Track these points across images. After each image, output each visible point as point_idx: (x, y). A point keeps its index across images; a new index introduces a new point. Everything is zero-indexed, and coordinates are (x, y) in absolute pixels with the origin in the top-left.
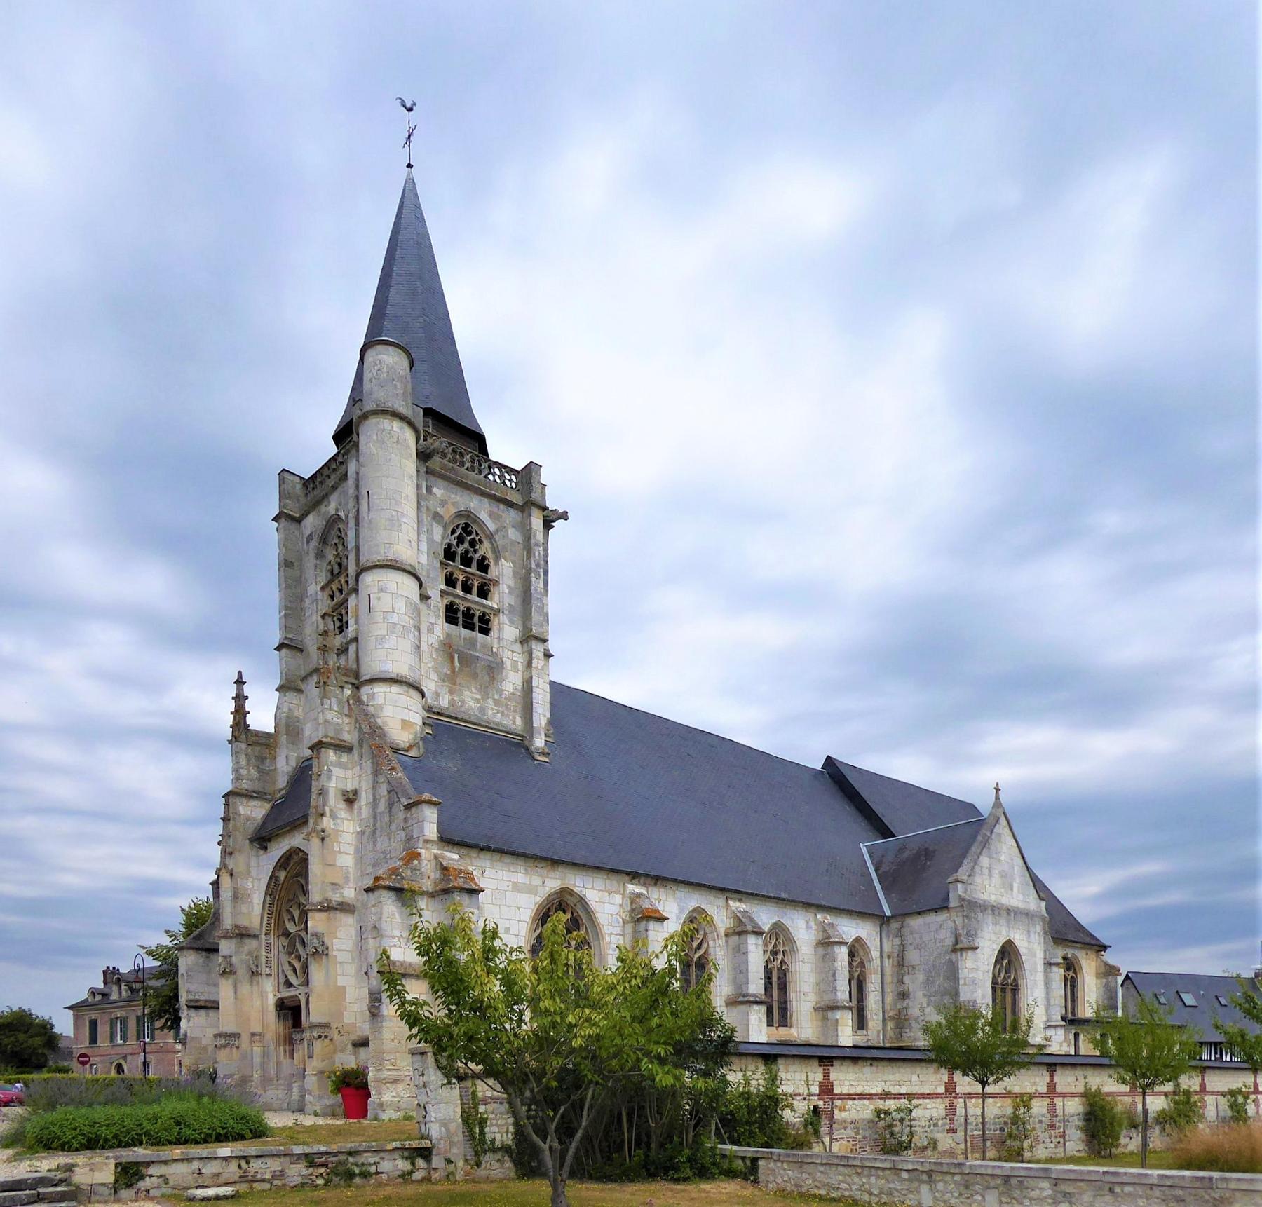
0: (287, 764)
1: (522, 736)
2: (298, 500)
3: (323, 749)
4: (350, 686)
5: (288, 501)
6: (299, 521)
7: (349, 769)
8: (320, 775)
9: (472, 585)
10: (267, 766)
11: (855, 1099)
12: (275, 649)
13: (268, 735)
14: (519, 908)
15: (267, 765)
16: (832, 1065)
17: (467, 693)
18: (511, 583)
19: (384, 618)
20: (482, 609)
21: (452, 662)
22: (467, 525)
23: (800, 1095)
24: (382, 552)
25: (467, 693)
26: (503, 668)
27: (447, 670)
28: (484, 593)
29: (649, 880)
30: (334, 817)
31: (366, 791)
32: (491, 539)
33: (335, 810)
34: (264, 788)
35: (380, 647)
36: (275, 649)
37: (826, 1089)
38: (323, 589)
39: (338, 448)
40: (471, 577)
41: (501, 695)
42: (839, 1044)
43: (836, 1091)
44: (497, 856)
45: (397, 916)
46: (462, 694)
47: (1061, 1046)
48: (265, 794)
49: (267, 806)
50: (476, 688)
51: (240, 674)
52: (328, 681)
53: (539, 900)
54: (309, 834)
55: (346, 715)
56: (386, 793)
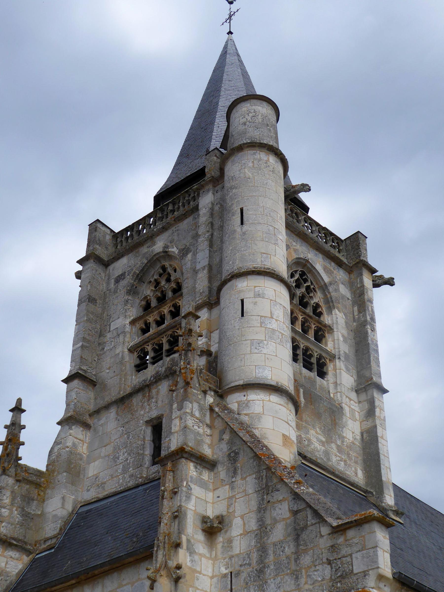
0: (63, 507)
1: (366, 492)
2: (107, 248)
3: (183, 460)
4: (212, 393)
5: (97, 246)
6: (106, 264)
7: (209, 490)
8: (175, 493)
9: (310, 328)
10: (33, 509)
12: (62, 381)
13: (39, 473)
15: (33, 508)
17: (312, 432)
18: (345, 332)
19: (261, 323)
20: (319, 352)
24: (259, 260)
25: (312, 432)
30: (191, 551)
31: (242, 517)
32: (324, 291)
33: (192, 541)
34: (25, 537)
35: (256, 351)
36: (62, 381)
38: (133, 323)
39: (82, 266)
40: (309, 319)
48: (26, 543)
49: (26, 559)
50: (321, 428)
51: (19, 401)
52: (191, 382)
54: (157, 571)
55: (207, 425)
56: (287, 515)
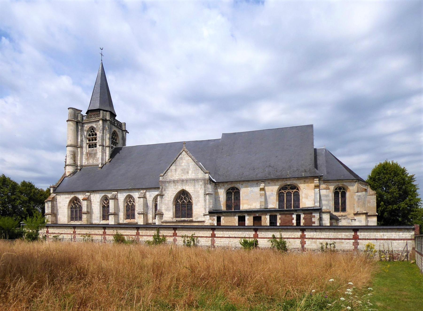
21: (88, 156)
22: (93, 128)
28: (96, 140)
29: (92, 192)
37: (47, 232)
44: (63, 193)
53: (70, 199)
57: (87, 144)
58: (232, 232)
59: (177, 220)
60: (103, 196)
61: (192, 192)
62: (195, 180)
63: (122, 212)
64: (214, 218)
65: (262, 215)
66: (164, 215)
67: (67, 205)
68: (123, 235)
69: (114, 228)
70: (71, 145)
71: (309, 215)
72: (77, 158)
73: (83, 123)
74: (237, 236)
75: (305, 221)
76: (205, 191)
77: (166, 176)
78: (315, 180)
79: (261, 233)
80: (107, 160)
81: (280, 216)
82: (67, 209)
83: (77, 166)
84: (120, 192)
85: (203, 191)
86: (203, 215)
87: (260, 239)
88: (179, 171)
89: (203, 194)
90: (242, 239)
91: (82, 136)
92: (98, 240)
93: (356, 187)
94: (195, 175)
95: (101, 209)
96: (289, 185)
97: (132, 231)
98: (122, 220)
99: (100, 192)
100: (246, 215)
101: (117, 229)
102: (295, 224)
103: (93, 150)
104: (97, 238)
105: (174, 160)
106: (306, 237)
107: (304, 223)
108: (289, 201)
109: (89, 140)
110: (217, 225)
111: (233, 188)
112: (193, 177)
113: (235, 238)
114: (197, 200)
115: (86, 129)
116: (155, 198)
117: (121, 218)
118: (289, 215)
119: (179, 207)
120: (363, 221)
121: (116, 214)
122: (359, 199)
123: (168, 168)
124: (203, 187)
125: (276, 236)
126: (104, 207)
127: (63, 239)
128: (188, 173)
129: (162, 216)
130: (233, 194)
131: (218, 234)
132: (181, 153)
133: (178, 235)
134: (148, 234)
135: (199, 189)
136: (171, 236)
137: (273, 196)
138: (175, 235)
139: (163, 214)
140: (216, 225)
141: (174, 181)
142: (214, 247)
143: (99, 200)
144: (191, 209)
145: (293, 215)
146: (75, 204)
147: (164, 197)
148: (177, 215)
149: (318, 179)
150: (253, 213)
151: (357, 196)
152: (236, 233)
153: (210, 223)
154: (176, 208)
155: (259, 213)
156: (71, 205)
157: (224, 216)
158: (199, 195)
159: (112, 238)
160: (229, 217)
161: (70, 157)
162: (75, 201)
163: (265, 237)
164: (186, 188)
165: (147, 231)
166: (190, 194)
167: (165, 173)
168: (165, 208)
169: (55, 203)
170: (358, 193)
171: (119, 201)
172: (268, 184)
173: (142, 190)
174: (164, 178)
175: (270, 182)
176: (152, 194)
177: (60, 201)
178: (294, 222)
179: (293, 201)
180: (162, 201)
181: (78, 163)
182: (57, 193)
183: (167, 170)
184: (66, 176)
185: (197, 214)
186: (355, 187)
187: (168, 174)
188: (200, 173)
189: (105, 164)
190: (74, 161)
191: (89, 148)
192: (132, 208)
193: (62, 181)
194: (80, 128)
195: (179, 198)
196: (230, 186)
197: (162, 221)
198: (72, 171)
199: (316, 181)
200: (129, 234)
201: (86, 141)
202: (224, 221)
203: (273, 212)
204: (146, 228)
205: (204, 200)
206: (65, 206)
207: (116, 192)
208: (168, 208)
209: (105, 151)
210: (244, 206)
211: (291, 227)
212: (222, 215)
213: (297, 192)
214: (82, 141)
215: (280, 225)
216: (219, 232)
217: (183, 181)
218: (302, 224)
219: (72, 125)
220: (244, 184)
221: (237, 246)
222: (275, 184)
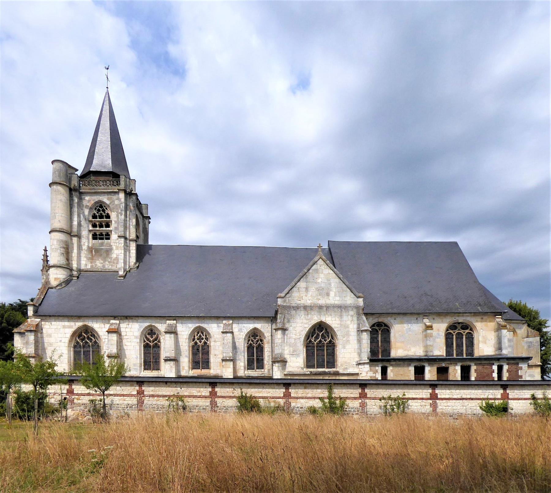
11: (85, 395)
14: (65, 333)
16: (73, 383)
22: (101, 205)
23: (57, 393)
26: (112, 249)
27: (90, 256)
28: (108, 226)
29: (122, 318)
41: (111, 259)
42: (165, 376)
43: (75, 392)
45: (19, 340)
46: (95, 262)
47: (367, 374)
50: (101, 259)
53: (73, 330)
57: (90, 231)
58: (465, 391)
59: (311, 372)
60: (146, 327)
61: (336, 326)
62: (341, 308)
63: (186, 356)
64: (377, 368)
65: (450, 365)
66: (288, 363)
67: (67, 340)
68: (255, 397)
69: (227, 384)
70: (61, 229)
71: (514, 367)
72: (70, 255)
73: (81, 193)
74: (474, 397)
75: (509, 375)
76: (359, 326)
77: (290, 298)
78: (497, 318)
79: (513, 391)
80: (133, 263)
81: (475, 366)
82: (66, 348)
83: (71, 270)
84: (180, 321)
85: (355, 326)
86: (355, 364)
87: (511, 401)
88: (312, 291)
89: (356, 330)
90: (484, 402)
91: (79, 216)
92: (196, 406)
93: (524, 330)
94: (341, 299)
95: (141, 350)
96: (459, 323)
97: (274, 390)
98: (186, 370)
99: (141, 320)
100: (426, 365)
101: (242, 387)
102: (496, 379)
103: (102, 244)
104: (196, 404)
105: (303, 273)
106: (439, 397)
107: (507, 378)
108: (460, 346)
109: (94, 226)
110: (382, 379)
111: (379, 324)
112: (336, 302)
113: (472, 399)
114: (344, 339)
115: (88, 204)
116: (248, 335)
117: (183, 367)
118: (488, 365)
119: (312, 351)
120: (536, 376)
121: (175, 360)
122: (529, 347)
123: (294, 284)
124: (355, 319)
125: (536, 396)
126: (146, 346)
127: (111, 407)
128: (328, 294)
129: (285, 365)
130: (380, 332)
131: (442, 394)
132: (316, 262)
133: (368, 396)
134: (309, 395)
135: (349, 322)
136: (355, 398)
137: (440, 338)
138: (363, 396)
139: (286, 362)
140: (380, 378)
141: (305, 308)
142: (437, 414)
143: (138, 333)
144: (332, 354)
145: (493, 366)
146: (82, 340)
147: (287, 332)
148: (310, 364)
149: (501, 317)
150: (438, 361)
151: (527, 342)
152: (473, 391)
153: (371, 377)
154: (307, 350)
155: (446, 362)
156: (74, 341)
157: (392, 365)
158: (348, 331)
159: (233, 402)
160: (400, 368)
161: (59, 251)
162: (83, 334)
163: (519, 397)
164: (327, 319)
165: (306, 390)
166: (334, 331)
167: (288, 293)
168: (290, 351)
169: (39, 335)
170: (527, 339)
171: (179, 336)
172: (433, 320)
173: (225, 320)
174: (285, 301)
175: (435, 318)
176: (244, 327)
177: (50, 331)
178: (495, 375)
179: (466, 347)
180: (284, 338)
181: (72, 264)
182: (44, 318)
183: (292, 288)
184: (50, 286)
185: (346, 362)
186: (523, 330)
187: (293, 294)
188: (349, 297)
189: (130, 271)
190: (68, 259)
191: (93, 239)
192: (204, 349)
193: (45, 295)
194: (76, 200)
195: (312, 336)
196: (376, 321)
197: (286, 373)
198: (64, 279)
199: (499, 319)
200: (269, 395)
201: (88, 227)
202: (392, 373)
203: (465, 361)
204: (305, 385)
205: (358, 340)
206: (62, 341)
207: (174, 320)
208: (294, 351)
209: (128, 248)
210: (399, 352)
211: (271, 381)
212: (389, 364)
213: (470, 333)
214: (79, 225)
215: (437, 379)
216: (444, 391)
217: (320, 307)
218: (505, 378)
219: (62, 193)
220: (398, 318)
221: (475, 412)
222: (442, 321)
